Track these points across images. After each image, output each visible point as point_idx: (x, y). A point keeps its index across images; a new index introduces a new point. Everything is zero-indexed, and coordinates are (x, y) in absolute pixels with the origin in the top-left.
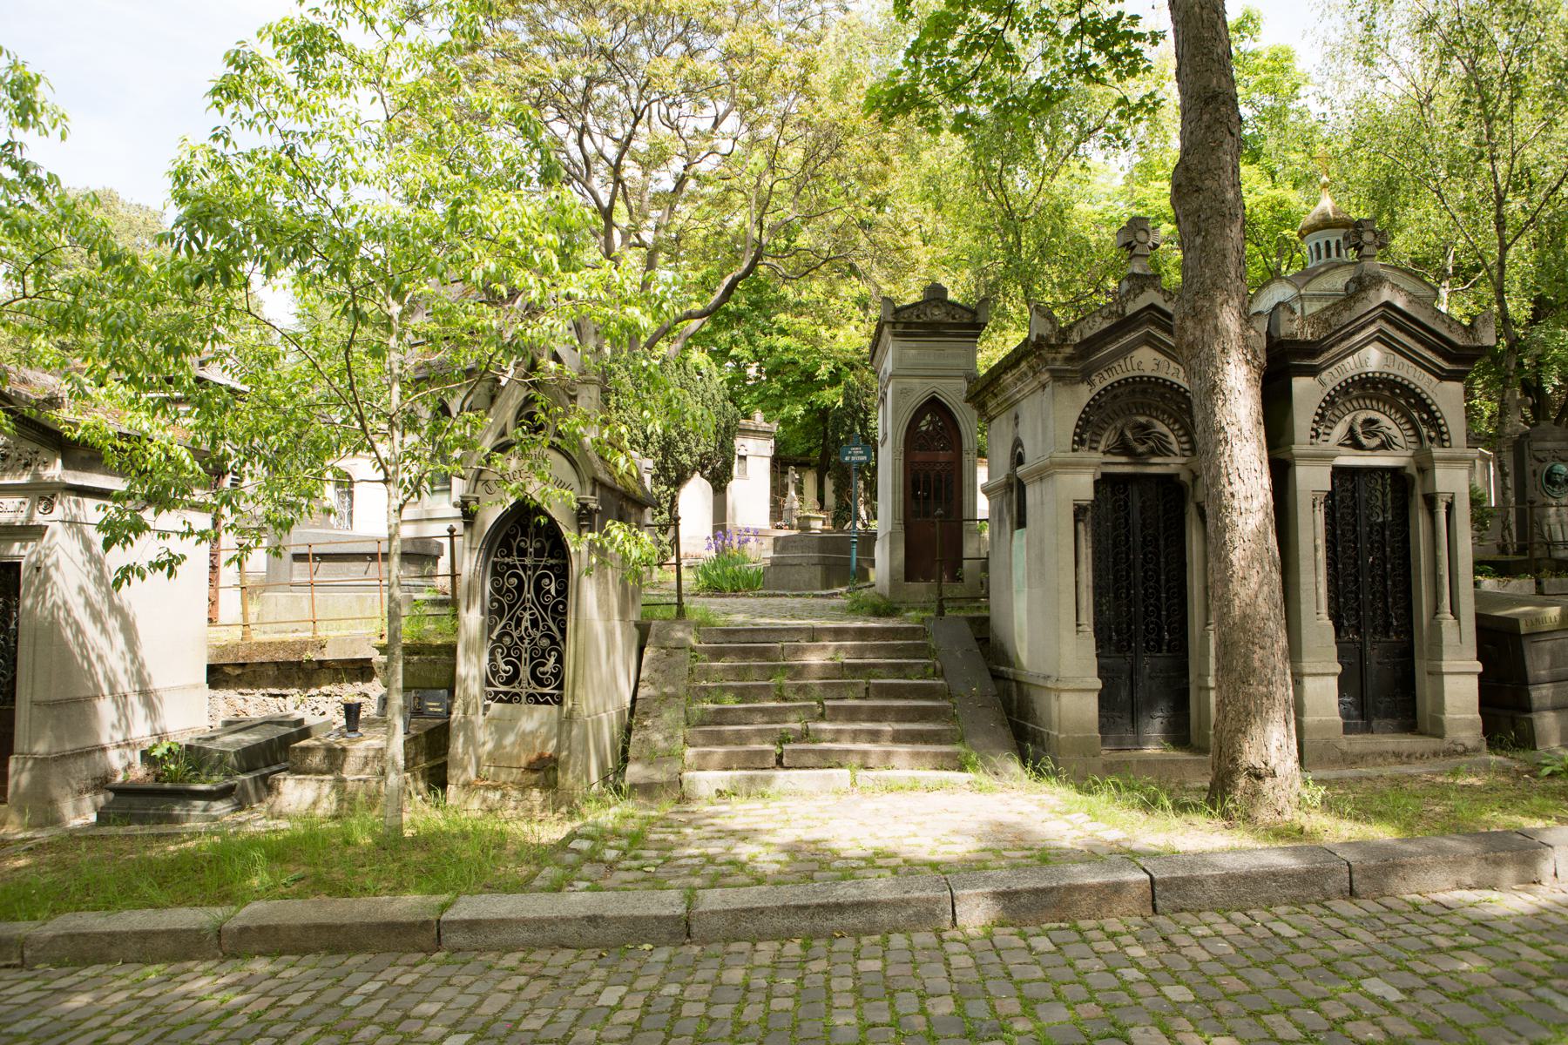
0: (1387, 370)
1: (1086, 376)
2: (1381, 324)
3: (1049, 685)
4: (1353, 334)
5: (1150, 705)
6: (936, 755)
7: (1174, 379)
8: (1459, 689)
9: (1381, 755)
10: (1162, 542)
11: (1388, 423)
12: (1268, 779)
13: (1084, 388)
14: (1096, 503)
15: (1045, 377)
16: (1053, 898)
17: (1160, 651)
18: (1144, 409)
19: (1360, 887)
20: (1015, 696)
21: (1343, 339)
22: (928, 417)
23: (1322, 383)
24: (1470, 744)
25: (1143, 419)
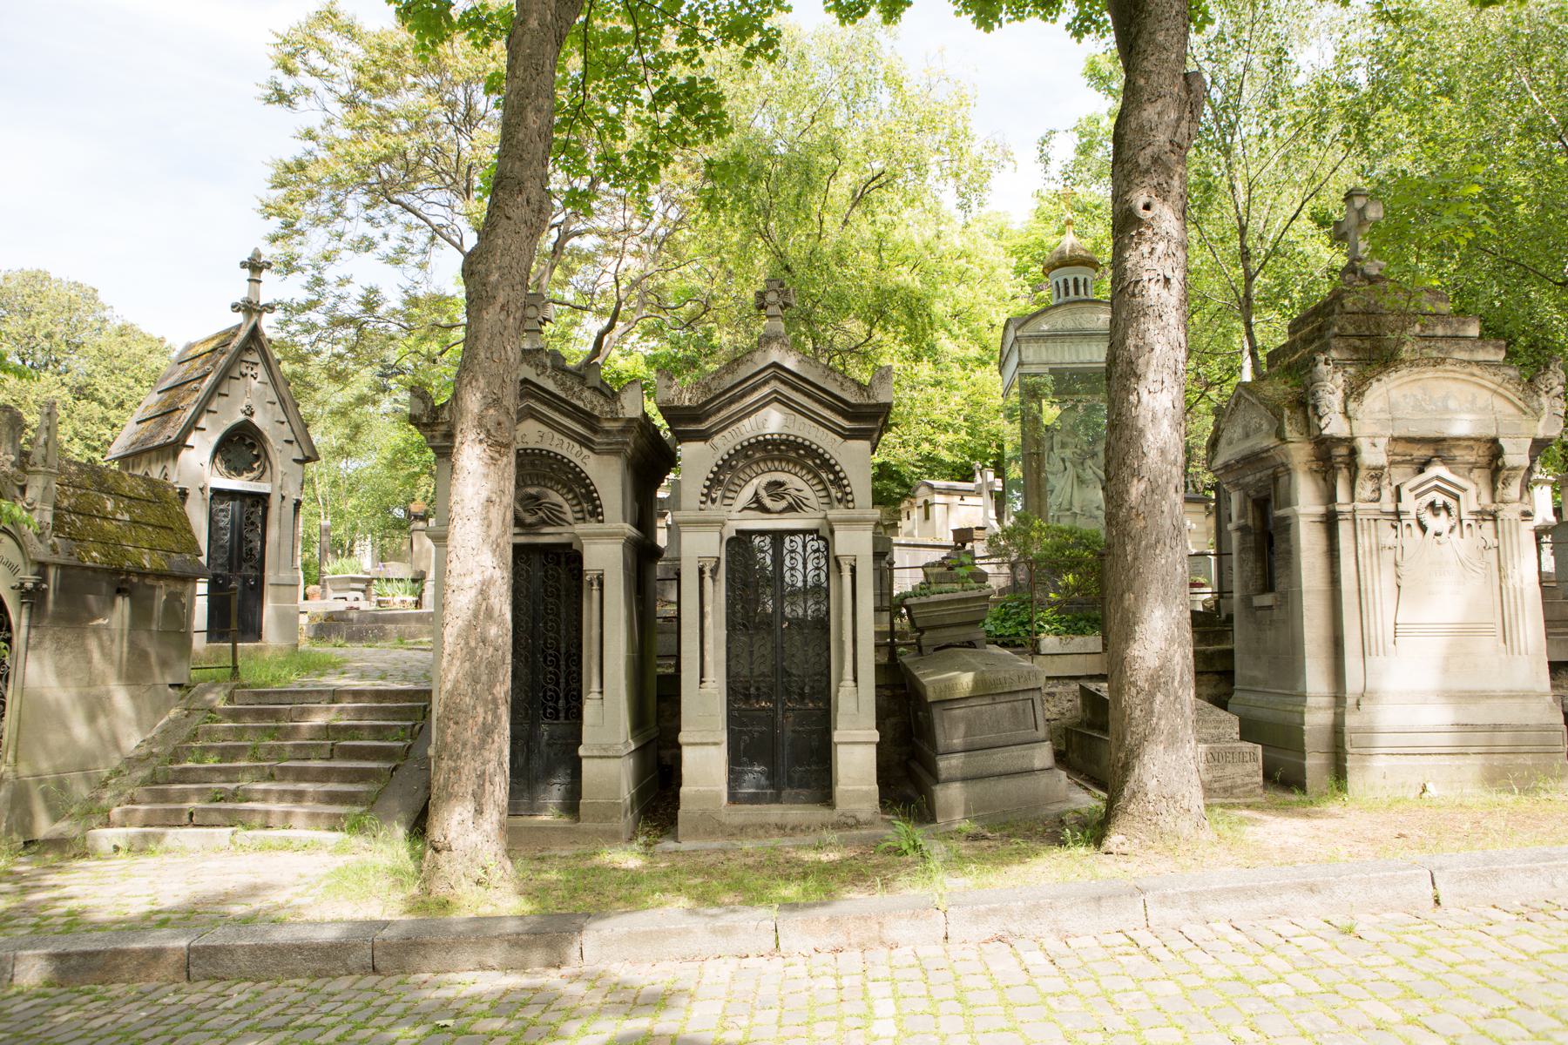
0: (787, 431)
2: (775, 384)
4: (743, 396)
5: (549, 773)
6: (330, 816)
7: (558, 451)
8: (856, 758)
9: (762, 827)
11: (796, 482)
12: (445, 853)
16: (98, 961)
17: (557, 718)
19: (380, 965)
21: (731, 402)
23: (714, 447)
24: (862, 817)
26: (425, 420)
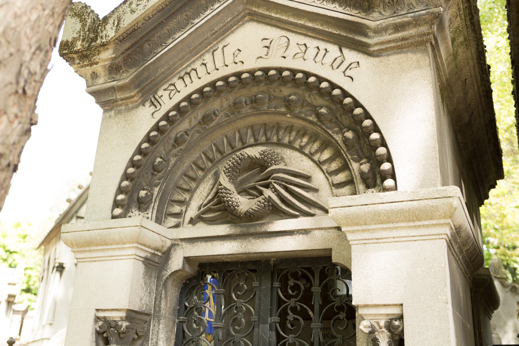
1: (146, 90)
13: (146, 110)
18: (269, 134)
25: (254, 152)
26: (79, 46)
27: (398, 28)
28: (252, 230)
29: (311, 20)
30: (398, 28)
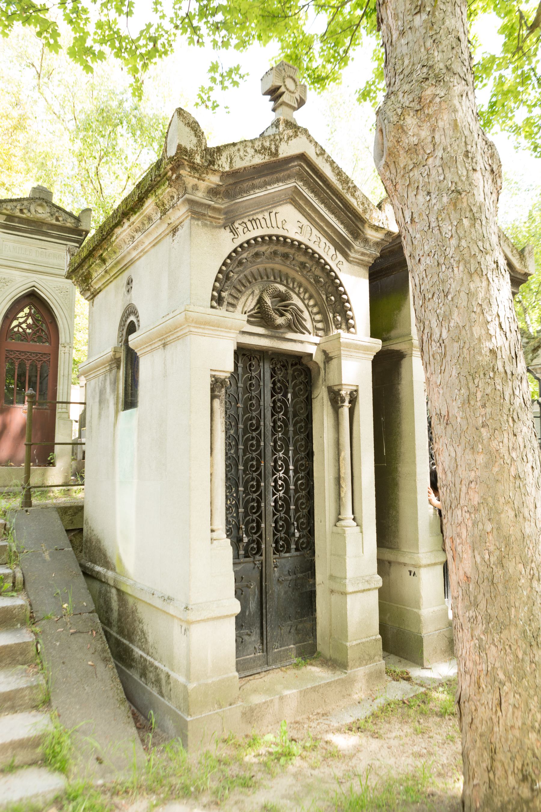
3: (171, 610)
10: (291, 428)
13: (226, 234)
14: (234, 375)
15: (180, 213)
20: (115, 605)
22: (27, 310)
25: (282, 288)
27: (363, 254)
28: (277, 335)
29: (327, 226)
30: (363, 254)
